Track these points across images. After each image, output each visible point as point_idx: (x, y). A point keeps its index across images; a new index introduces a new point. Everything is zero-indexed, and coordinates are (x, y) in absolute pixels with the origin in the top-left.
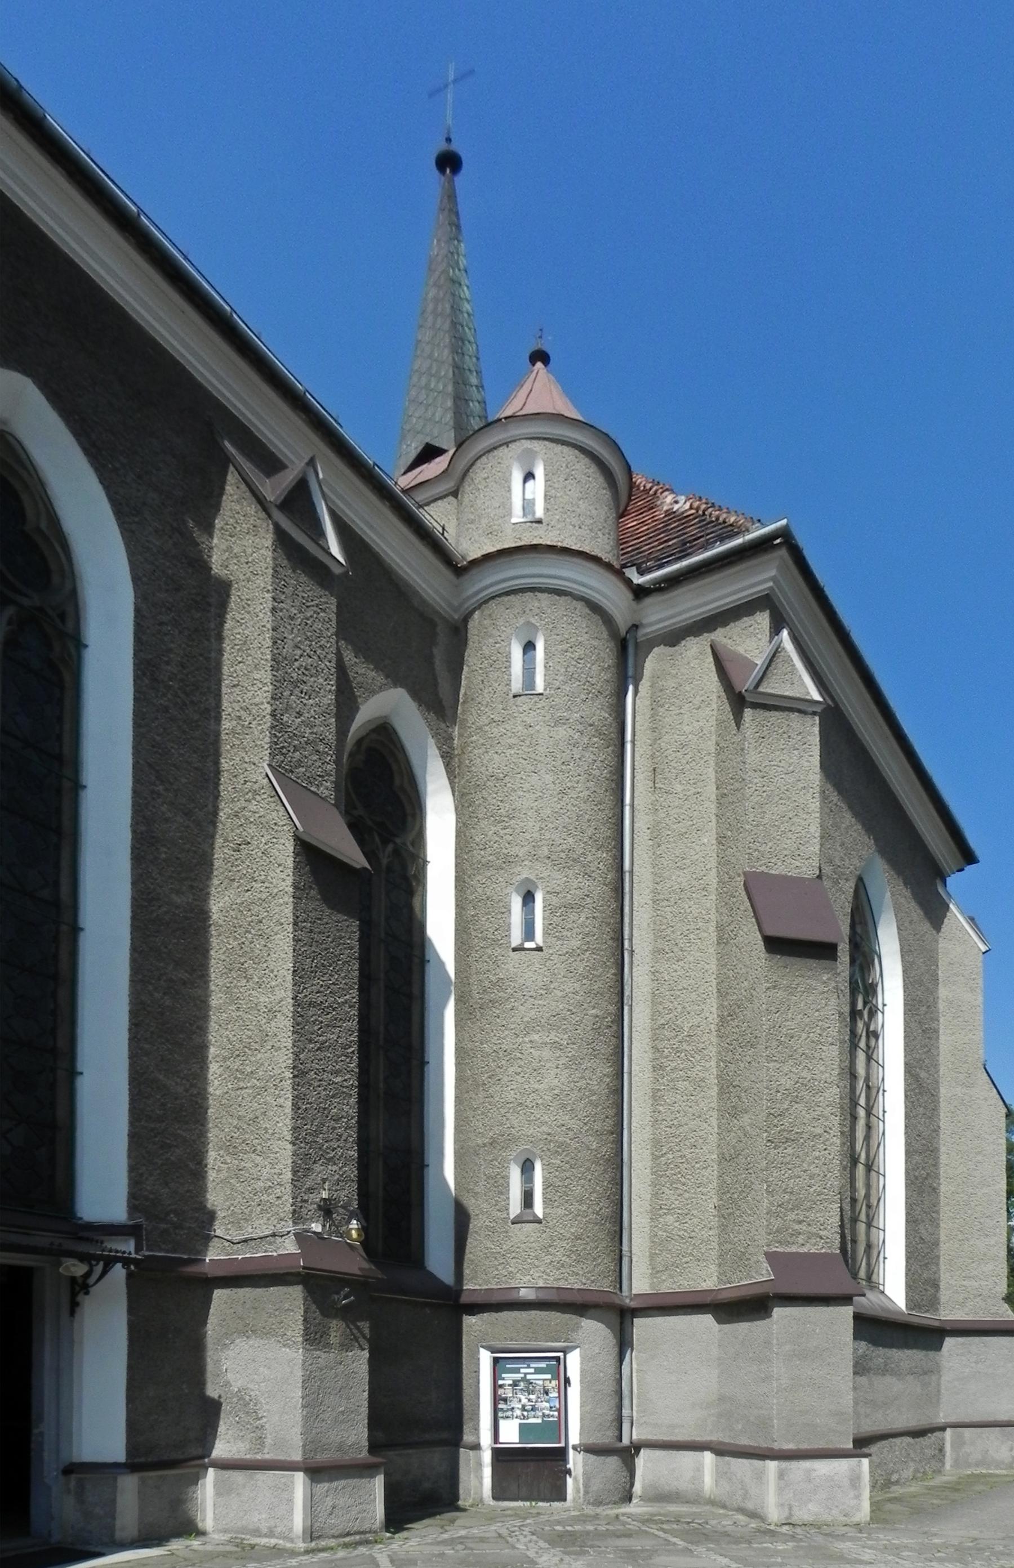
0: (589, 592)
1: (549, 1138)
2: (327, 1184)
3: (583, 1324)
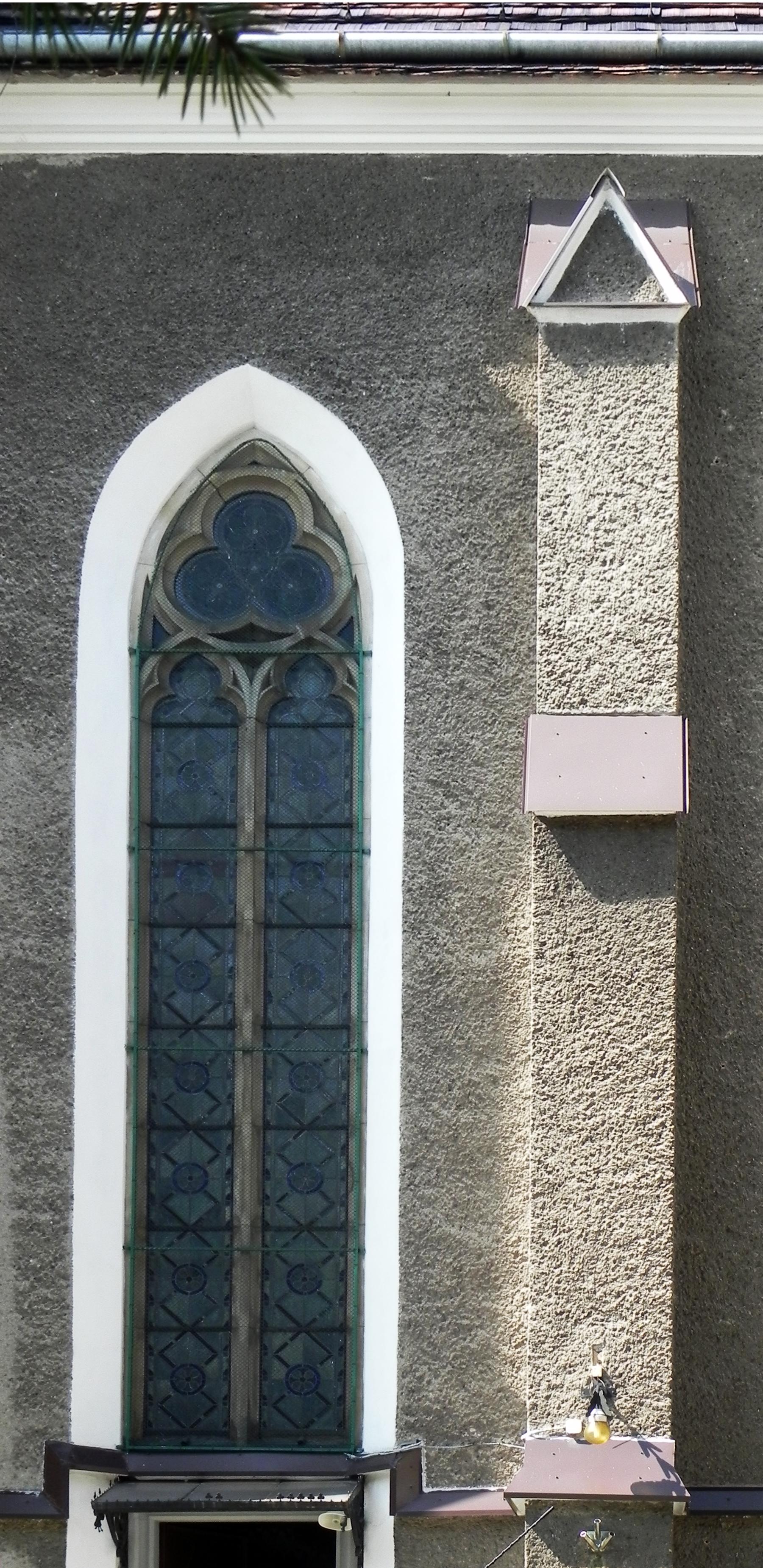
2: (605, 1351)
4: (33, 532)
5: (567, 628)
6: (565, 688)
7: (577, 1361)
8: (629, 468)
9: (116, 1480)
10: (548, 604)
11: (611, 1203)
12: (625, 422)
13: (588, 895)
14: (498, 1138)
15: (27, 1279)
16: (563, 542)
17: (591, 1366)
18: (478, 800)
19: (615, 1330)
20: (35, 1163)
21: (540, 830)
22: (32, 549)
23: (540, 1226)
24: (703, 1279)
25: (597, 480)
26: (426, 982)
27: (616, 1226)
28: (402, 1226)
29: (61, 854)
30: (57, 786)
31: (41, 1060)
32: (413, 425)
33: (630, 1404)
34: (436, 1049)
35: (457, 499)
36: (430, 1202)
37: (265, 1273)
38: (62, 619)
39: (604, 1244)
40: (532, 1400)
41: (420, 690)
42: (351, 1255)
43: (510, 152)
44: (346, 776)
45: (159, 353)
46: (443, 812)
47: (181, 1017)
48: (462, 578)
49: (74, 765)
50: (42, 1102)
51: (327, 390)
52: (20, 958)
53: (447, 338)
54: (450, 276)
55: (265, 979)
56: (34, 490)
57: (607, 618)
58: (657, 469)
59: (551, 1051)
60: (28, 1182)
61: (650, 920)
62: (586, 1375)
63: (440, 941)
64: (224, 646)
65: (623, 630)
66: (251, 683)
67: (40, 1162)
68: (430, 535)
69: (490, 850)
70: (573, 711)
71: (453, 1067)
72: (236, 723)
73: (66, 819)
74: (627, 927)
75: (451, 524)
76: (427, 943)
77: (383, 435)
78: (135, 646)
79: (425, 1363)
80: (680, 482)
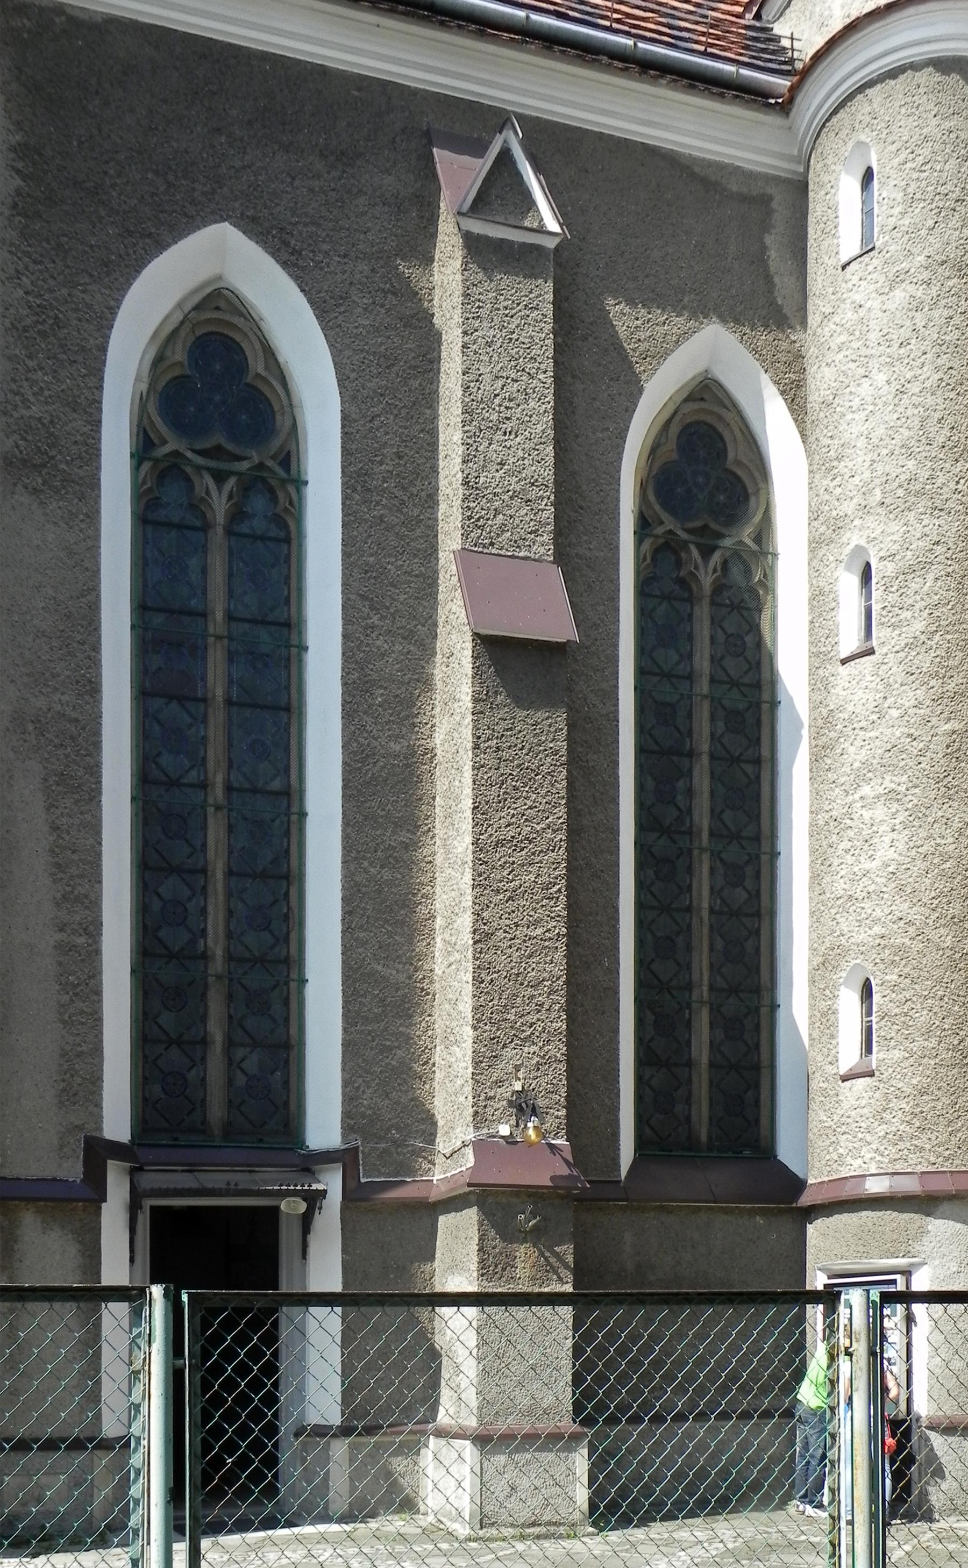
0: (926, 48)
1: (883, 942)
2: (522, 1070)
3: (930, 1228)
4: (66, 338)
11: (526, 951)
14: (408, 894)
15: (67, 993)
18: (393, 615)
22: (65, 353)
25: (500, 365)
27: (529, 970)
28: (343, 962)
29: (90, 624)
30: (87, 564)
34: (365, 819)
38: (90, 419)
42: (293, 985)
45: (161, 199)
47: (167, 776)
50: (77, 839)
51: (285, 256)
52: (59, 712)
53: (369, 230)
54: (371, 178)
56: (66, 302)
60: (67, 909)
61: (550, 726)
62: (510, 1089)
64: (199, 460)
66: (220, 494)
67: (76, 892)
68: (358, 391)
70: (485, 551)
71: (377, 833)
72: (206, 527)
76: (359, 729)
77: (325, 302)
79: (361, 1076)
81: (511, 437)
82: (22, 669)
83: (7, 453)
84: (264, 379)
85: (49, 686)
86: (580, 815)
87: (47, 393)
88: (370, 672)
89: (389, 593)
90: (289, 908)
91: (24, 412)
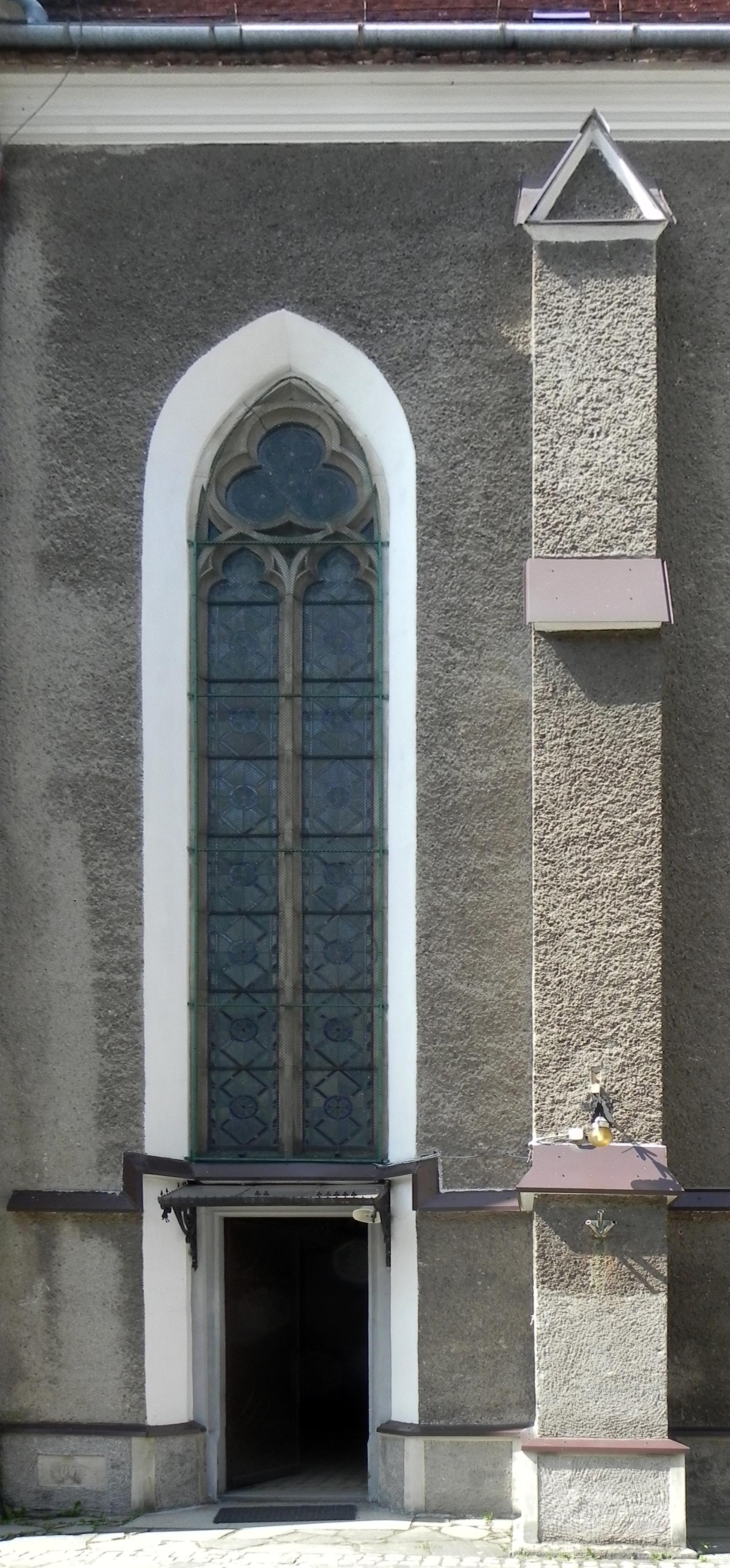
2: (602, 1072)
4: (105, 442)
5: (560, 488)
6: (558, 537)
7: (578, 1081)
8: (614, 358)
9: (184, 1184)
10: (543, 468)
11: (606, 949)
12: (610, 321)
13: (583, 695)
14: (498, 914)
15: (107, 1025)
16: (555, 418)
17: (590, 1085)
19: (611, 1055)
20: (111, 935)
21: (539, 642)
23: (543, 969)
24: (675, 1025)
25: (585, 368)
26: (437, 792)
28: (418, 983)
30: (127, 640)
31: (116, 854)
32: (422, 356)
33: (626, 1116)
35: (460, 413)
36: (442, 965)
37: (306, 1026)
39: (600, 984)
40: (538, 1112)
41: (430, 563)
42: (376, 1011)
43: (504, 140)
44: (369, 642)
46: (450, 658)
47: (330, 1062)
48: (465, 475)
49: (140, 623)
50: (117, 887)
52: (97, 775)
53: (451, 287)
55: (303, 798)
56: (106, 409)
57: (594, 479)
58: (638, 358)
59: (551, 824)
60: (106, 950)
61: (638, 716)
62: (586, 1092)
63: (448, 759)
64: (267, 539)
65: (609, 489)
66: (289, 567)
67: (115, 935)
68: (438, 441)
69: (490, 688)
70: (565, 555)
71: (460, 858)
73: (135, 666)
74: (618, 722)
75: (455, 433)
76: (438, 761)
78: (193, 539)
79: (440, 1092)
80: (658, 369)
81: (600, 438)
82: (60, 741)
83: (43, 552)
84: (341, 456)
85: (86, 753)
86: (718, 823)
87: (84, 494)
88: (451, 706)
89: (474, 629)
90: (372, 940)
91: (61, 514)
